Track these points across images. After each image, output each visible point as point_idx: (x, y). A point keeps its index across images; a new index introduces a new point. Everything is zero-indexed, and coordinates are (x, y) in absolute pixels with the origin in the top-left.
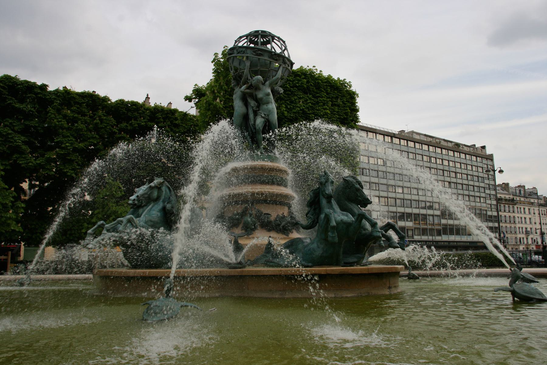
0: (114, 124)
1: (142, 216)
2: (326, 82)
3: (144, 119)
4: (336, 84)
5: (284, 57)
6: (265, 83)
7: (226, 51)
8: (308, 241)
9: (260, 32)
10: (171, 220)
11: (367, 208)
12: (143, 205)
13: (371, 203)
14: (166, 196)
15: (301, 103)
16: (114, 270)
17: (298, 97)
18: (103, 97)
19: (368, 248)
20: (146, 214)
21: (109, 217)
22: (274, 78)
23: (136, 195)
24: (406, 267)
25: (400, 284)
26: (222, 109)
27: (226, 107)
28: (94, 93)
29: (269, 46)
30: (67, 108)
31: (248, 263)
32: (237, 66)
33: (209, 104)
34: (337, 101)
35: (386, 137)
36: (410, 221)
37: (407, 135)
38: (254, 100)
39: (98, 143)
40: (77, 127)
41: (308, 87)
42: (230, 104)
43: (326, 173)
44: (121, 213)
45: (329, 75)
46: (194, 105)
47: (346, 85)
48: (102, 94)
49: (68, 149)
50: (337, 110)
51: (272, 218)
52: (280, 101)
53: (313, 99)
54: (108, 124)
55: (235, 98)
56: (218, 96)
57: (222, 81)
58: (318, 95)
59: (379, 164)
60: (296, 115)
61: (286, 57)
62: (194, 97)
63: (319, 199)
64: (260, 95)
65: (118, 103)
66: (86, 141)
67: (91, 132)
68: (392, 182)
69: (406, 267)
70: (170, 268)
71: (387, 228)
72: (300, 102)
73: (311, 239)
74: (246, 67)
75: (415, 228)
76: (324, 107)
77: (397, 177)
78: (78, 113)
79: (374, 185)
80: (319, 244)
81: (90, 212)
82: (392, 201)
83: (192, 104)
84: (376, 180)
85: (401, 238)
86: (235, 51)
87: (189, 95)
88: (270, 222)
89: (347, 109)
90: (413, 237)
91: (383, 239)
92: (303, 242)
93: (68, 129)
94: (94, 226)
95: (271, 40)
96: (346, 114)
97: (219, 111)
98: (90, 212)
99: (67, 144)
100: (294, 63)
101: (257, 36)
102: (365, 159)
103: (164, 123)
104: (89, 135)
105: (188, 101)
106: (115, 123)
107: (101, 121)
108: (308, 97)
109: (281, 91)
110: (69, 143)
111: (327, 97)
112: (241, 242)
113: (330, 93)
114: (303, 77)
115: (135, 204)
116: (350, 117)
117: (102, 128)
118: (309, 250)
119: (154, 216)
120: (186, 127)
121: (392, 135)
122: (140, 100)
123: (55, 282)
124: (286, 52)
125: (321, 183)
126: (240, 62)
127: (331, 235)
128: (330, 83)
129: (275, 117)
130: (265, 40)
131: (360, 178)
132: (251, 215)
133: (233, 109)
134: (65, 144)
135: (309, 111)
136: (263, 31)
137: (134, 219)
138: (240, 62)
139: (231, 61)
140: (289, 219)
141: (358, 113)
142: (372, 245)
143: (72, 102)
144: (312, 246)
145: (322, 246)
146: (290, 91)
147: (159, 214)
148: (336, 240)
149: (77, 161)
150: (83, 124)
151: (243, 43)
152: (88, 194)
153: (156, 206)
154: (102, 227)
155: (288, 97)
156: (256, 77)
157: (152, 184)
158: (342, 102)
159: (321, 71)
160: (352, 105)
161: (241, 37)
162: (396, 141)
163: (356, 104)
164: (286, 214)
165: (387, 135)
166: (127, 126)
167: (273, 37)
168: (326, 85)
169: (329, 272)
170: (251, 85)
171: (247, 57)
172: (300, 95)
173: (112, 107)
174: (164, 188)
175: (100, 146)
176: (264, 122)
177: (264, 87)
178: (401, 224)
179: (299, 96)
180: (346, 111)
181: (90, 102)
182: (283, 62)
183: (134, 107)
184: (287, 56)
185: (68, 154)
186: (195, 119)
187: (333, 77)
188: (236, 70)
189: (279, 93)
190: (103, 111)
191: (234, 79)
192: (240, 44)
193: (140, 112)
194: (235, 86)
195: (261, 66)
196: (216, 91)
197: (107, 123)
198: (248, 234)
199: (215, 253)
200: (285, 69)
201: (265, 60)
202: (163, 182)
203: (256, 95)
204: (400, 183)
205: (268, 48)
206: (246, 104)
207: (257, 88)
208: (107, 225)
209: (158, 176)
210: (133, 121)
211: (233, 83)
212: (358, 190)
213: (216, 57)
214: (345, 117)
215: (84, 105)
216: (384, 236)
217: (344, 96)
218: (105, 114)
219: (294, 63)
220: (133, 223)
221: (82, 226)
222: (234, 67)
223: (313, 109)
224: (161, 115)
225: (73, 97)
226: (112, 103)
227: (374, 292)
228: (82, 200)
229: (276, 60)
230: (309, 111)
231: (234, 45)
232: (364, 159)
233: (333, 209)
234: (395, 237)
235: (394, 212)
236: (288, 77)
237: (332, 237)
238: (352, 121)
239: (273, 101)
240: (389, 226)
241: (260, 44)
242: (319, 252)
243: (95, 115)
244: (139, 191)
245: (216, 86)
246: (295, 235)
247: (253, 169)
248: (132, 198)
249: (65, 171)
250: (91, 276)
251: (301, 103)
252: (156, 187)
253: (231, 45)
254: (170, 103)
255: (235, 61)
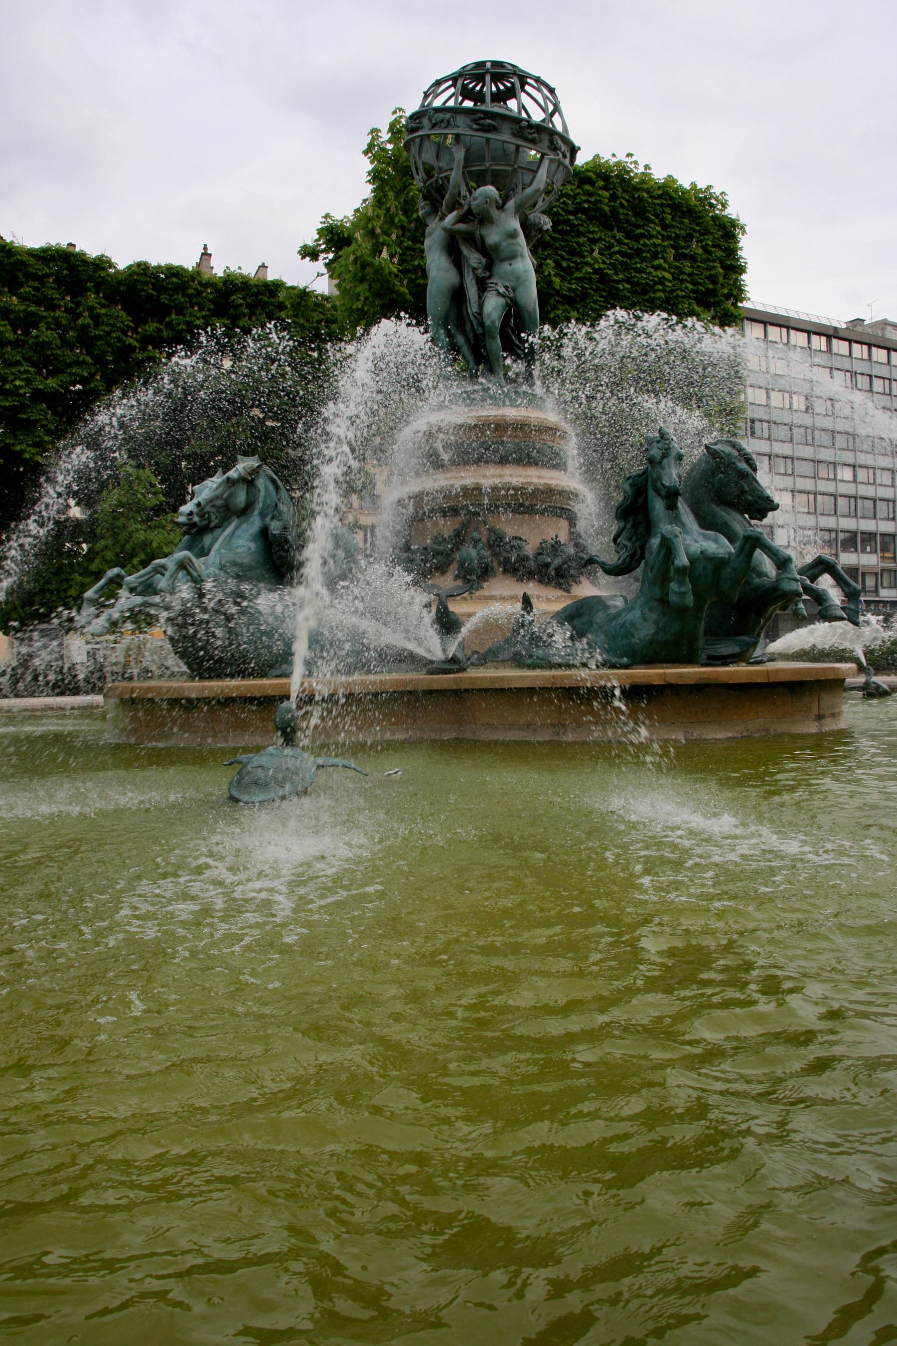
0: (128, 326)
1: (212, 553)
2: (660, 197)
3: (201, 310)
4: (687, 201)
5: (552, 133)
6: (504, 203)
7: (399, 122)
8: (619, 603)
9: (489, 65)
10: (9, 525)
11: (765, 521)
12: (212, 525)
13: (775, 507)
14: (269, 502)
15: (596, 254)
16: (153, 683)
17: (589, 239)
18: (95, 259)
19: (767, 620)
20: (222, 546)
21: (130, 556)
22: (529, 191)
23: (195, 501)
24: (861, 669)
25: (845, 708)
26: (396, 276)
27: (404, 272)
28: (71, 249)
29: (512, 104)
30: (10, 291)
31: (472, 660)
32: (433, 161)
33: (362, 264)
34: (689, 247)
35: (814, 338)
36: (871, 552)
37: (870, 331)
38: (477, 249)
39: (92, 375)
40: (37, 337)
41: (613, 211)
42: (416, 263)
43: (663, 435)
44: (160, 547)
45: (670, 176)
46: (324, 270)
47: (713, 201)
48: (92, 251)
49: (21, 395)
50: (688, 270)
51: (529, 550)
52: (543, 250)
53: (626, 241)
54: (114, 326)
55: (430, 249)
56: (383, 244)
57: (393, 204)
58: (639, 231)
59: (795, 407)
60: (583, 287)
61: (557, 133)
62: (323, 247)
63: (646, 501)
64: (493, 237)
65: (134, 273)
66: (63, 372)
67: (72, 350)
68: (826, 455)
69: (861, 669)
70: (287, 675)
71: (816, 571)
72: (593, 250)
73: (625, 599)
74: (456, 163)
75: (882, 570)
76: (657, 262)
77: (840, 441)
78: (38, 303)
79: (782, 461)
80: (646, 610)
81: (84, 546)
82: (825, 503)
83: (320, 266)
84: (785, 449)
85: (851, 595)
86: (425, 122)
87: (311, 243)
88: (524, 559)
89: (715, 267)
90: (876, 591)
91: (805, 597)
92: (606, 607)
93: (17, 344)
94: (98, 579)
95: (518, 85)
96: (713, 279)
97: (388, 282)
98: (84, 546)
99: (17, 383)
100: (579, 149)
101: (480, 78)
102: (758, 396)
103: (250, 319)
104: (69, 355)
105: (308, 259)
106: (131, 324)
107: (96, 319)
108: (614, 237)
109: (546, 223)
110: (22, 380)
111: (663, 236)
112: (456, 608)
113: (672, 226)
114: (601, 183)
115: (194, 525)
116: (723, 286)
117: (99, 337)
118: (622, 626)
119: (239, 550)
120: (307, 325)
121: (831, 333)
122: (188, 261)
123: (33, 715)
124: (556, 119)
125: (651, 461)
126: (440, 149)
127: (677, 590)
128: (671, 198)
129: (530, 295)
130: (502, 87)
131: (751, 446)
132: (476, 542)
133: (425, 275)
134: (12, 381)
135: (617, 274)
136: (497, 64)
137: (194, 559)
138: (440, 149)
139: (414, 150)
140: (571, 550)
141: (743, 277)
142: (778, 612)
143: (20, 275)
144: (628, 617)
145: (654, 616)
146: (567, 222)
147: (253, 546)
148: (690, 600)
149: (45, 422)
150: (51, 329)
151: (445, 98)
152: (78, 504)
153: (244, 526)
154: (117, 582)
155: (564, 240)
156: (482, 189)
157: (233, 474)
158: (703, 247)
159: (647, 167)
160: (728, 256)
161: (438, 83)
162: (840, 347)
163: (739, 253)
164: (563, 537)
165: (815, 333)
166: (159, 330)
167: (523, 78)
168: (661, 205)
169: (673, 681)
170: (470, 211)
171: (457, 137)
172: (592, 233)
173: (120, 283)
174: (261, 483)
175: (97, 382)
176: (504, 309)
177: (503, 215)
178: (847, 559)
179: (591, 236)
180: (712, 272)
181: (65, 272)
182: (549, 148)
183: (174, 280)
184: (559, 128)
185: (22, 407)
186: (329, 305)
187: (679, 183)
188: (429, 172)
189: (540, 230)
190: (97, 293)
191: (425, 198)
192: (438, 103)
193: (191, 291)
194: (427, 214)
195: (494, 159)
196: (378, 231)
197: (110, 325)
198: (471, 590)
199: (412, 646)
200: (555, 165)
201: (504, 142)
202: (259, 467)
203: (482, 239)
204: (849, 457)
205: (511, 111)
206: (457, 261)
207: (485, 219)
208: (128, 579)
209: (245, 454)
210: (173, 316)
211: (423, 208)
212: (743, 475)
213: (373, 139)
214: (711, 286)
215: (51, 280)
216: (807, 590)
217: (707, 232)
218: (103, 301)
219: (579, 149)
220: (191, 570)
221: (67, 580)
222: (424, 163)
223: (627, 269)
224: (244, 299)
225: (23, 263)
226: (118, 272)
227: (782, 727)
228: (63, 517)
229: (533, 141)
230: (617, 274)
231: (423, 105)
232: (755, 396)
233: (683, 525)
234: (835, 596)
235: (830, 531)
236: (563, 185)
237: (680, 593)
238: (728, 296)
239: (526, 251)
240: (821, 566)
241: (488, 98)
242: (645, 632)
243: (78, 304)
244: (200, 492)
245: (378, 216)
246: (586, 589)
247: (480, 427)
248: (185, 509)
249: (18, 448)
250: (99, 699)
251: (596, 254)
252: (242, 480)
253: (412, 106)
254: (263, 266)
255: (425, 149)
